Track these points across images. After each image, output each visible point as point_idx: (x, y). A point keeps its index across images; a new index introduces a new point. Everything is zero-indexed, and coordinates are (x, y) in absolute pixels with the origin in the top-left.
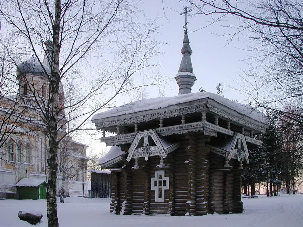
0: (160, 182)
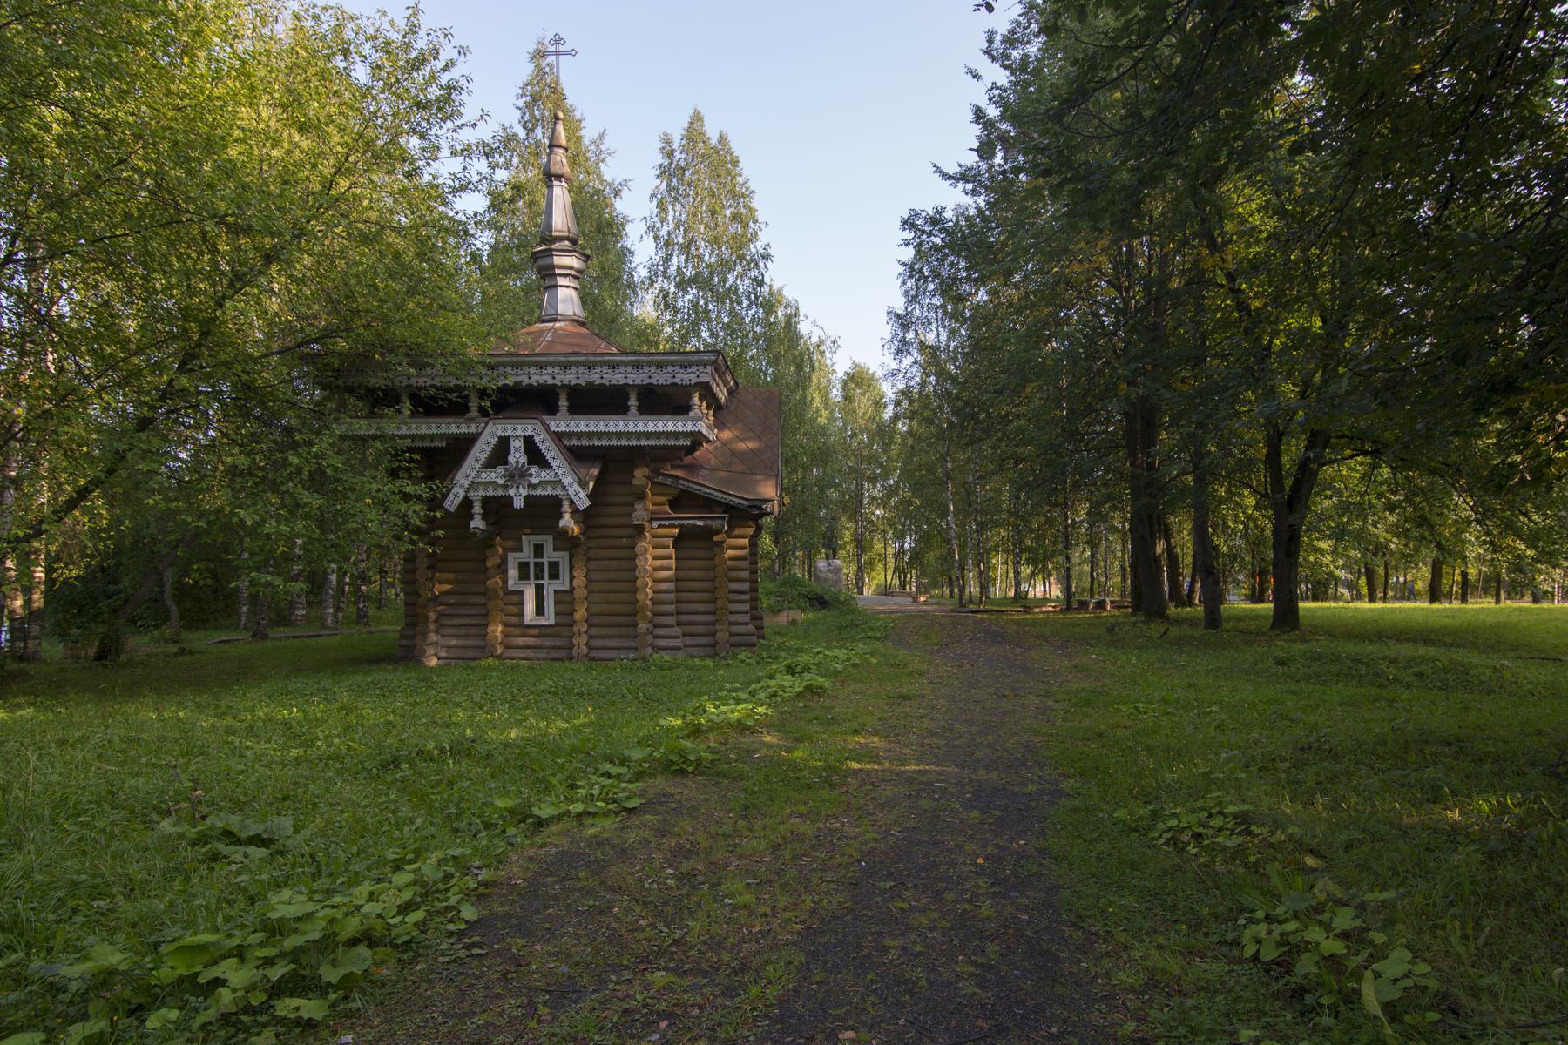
0: (539, 567)
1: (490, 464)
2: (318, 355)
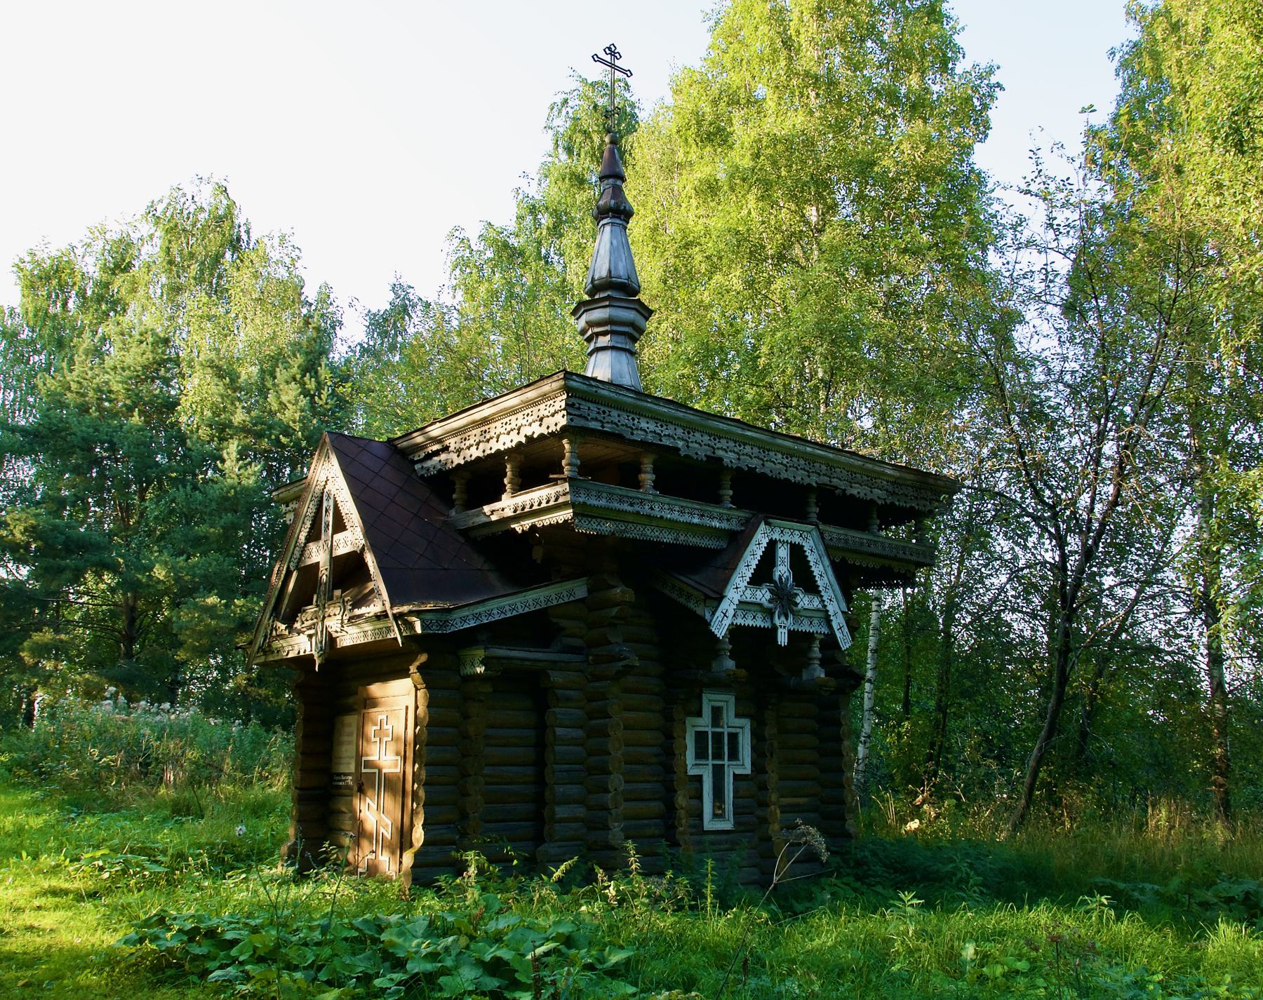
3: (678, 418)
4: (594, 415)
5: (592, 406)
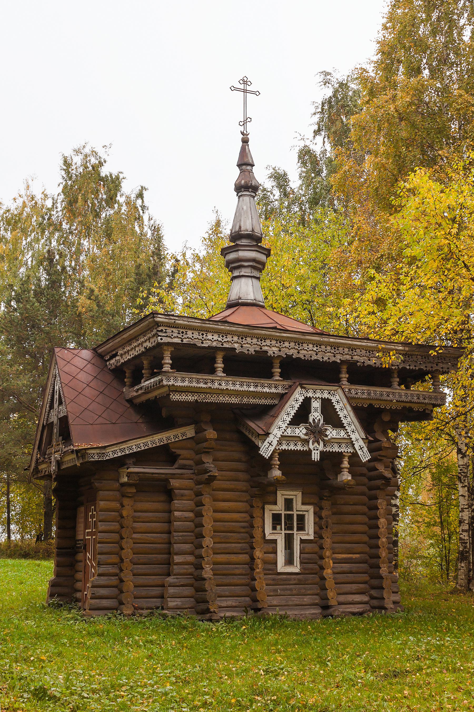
1: (295, 421)
2: (28, 317)
3: (232, 331)
4: (175, 335)
5: (174, 330)
